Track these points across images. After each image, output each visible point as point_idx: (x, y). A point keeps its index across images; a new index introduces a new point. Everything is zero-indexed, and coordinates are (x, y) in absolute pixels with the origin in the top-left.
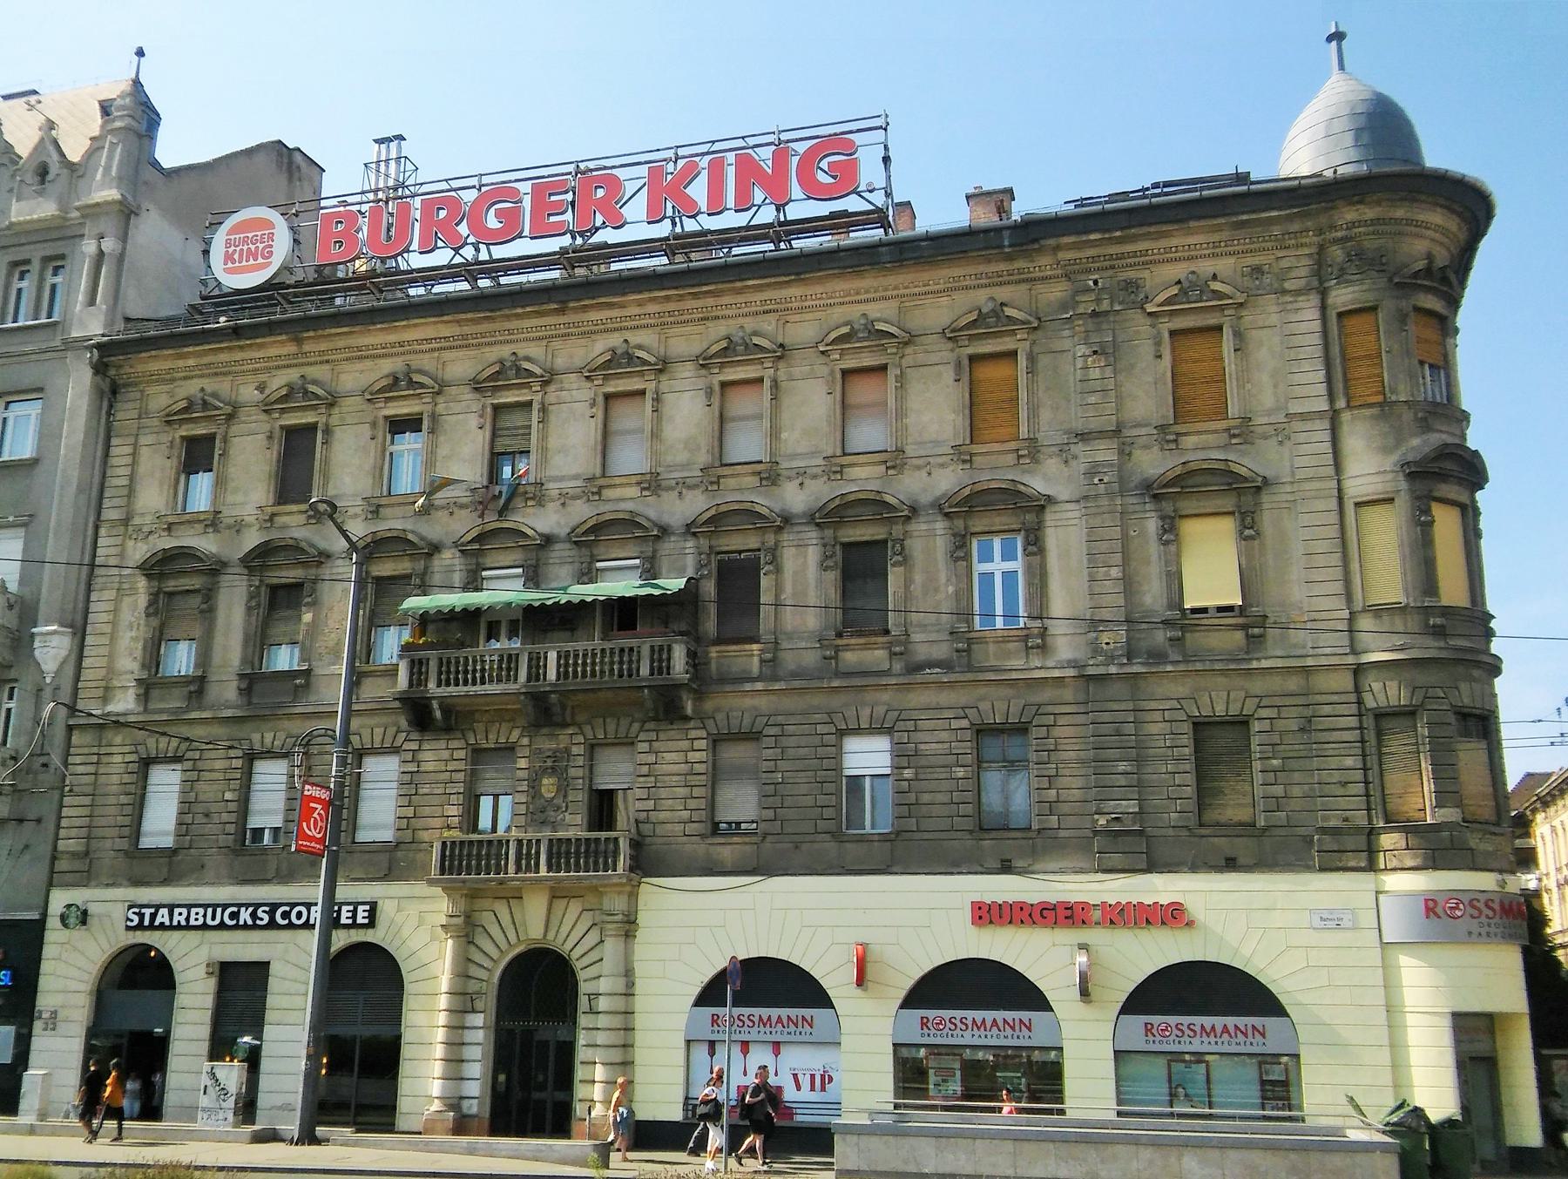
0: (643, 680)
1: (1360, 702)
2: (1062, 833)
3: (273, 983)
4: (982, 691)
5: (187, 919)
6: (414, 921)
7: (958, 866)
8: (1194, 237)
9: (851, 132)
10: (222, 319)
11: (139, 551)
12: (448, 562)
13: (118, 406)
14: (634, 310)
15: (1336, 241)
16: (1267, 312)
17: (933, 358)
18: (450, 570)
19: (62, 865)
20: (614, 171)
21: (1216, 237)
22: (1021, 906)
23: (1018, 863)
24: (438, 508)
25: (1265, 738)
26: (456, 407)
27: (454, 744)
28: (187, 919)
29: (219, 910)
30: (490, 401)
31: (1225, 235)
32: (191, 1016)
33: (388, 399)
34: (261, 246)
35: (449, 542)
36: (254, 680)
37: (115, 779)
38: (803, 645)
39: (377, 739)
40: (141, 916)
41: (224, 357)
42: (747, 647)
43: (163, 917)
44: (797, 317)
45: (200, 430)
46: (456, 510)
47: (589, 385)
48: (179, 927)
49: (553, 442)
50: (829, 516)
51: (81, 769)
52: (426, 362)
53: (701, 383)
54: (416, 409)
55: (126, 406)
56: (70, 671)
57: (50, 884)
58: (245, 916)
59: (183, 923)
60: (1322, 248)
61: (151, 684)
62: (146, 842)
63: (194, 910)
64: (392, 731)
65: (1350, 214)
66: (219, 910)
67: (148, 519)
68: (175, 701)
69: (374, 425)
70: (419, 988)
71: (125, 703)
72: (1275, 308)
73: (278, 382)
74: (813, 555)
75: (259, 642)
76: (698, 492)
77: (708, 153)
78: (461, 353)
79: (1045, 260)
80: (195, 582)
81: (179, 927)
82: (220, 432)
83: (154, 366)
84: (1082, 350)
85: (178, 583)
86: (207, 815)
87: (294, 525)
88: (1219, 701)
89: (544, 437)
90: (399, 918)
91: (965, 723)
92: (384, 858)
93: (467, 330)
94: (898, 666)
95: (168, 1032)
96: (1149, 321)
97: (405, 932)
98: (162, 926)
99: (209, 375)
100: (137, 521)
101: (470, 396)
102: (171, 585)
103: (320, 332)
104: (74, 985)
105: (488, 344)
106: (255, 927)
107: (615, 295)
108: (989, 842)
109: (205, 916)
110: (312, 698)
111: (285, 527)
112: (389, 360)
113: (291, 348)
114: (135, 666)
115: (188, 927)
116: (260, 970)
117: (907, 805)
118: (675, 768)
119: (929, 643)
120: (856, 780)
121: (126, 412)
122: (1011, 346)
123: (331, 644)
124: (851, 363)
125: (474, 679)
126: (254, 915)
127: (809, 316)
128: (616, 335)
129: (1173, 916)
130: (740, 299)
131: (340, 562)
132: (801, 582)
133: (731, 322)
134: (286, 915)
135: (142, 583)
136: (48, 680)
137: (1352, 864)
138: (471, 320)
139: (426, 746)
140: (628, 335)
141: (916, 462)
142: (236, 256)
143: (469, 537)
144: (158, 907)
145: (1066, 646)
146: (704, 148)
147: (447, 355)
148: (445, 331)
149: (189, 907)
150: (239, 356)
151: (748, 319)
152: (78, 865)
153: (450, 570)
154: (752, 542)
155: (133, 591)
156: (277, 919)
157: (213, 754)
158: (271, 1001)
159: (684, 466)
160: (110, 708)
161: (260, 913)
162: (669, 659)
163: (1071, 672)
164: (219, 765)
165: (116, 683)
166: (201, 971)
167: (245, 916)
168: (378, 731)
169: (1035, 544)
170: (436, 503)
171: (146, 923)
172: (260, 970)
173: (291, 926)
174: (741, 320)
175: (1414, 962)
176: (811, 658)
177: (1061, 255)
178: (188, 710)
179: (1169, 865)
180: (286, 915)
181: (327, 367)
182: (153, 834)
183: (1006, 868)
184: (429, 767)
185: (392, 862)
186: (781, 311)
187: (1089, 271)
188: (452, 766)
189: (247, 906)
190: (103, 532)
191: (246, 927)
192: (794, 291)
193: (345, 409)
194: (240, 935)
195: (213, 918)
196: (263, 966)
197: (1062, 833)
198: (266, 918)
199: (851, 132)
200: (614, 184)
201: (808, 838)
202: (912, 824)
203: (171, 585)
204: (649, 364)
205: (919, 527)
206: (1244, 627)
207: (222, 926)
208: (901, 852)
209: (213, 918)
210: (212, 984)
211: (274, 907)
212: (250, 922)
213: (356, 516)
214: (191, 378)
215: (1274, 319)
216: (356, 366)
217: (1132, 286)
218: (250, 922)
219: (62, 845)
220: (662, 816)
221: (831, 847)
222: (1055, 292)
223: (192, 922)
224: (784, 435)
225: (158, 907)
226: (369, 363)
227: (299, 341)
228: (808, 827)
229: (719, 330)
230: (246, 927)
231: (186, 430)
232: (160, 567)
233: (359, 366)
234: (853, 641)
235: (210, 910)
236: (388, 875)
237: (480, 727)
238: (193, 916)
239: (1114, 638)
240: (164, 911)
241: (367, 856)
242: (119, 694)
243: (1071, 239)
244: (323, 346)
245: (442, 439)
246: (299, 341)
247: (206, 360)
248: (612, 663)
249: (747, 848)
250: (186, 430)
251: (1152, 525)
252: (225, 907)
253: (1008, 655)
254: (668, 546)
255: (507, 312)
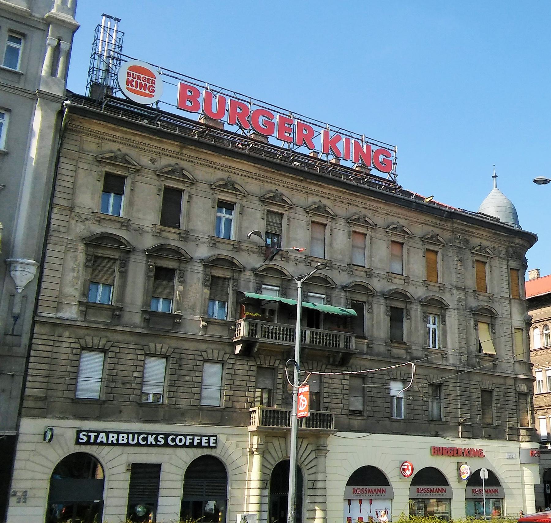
0: (307, 345)
1: (515, 389)
2: (451, 424)
3: (163, 475)
4: (430, 370)
5: (118, 440)
6: (234, 446)
7: (423, 433)
8: (484, 233)
9: (343, 134)
10: (146, 121)
11: (79, 229)
12: (248, 277)
13: (66, 140)
14: (328, 191)
15: (512, 247)
16: (495, 262)
17: (417, 246)
18: (248, 281)
19: (28, 403)
20: (389, 151)
21: (489, 235)
22: (445, 449)
23: (440, 433)
24: (243, 250)
25: (498, 397)
26: (252, 206)
27: (251, 363)
28: (118, 440)
29: (136, 436)
30: (266, 208)
31: (491, 235)
32: (116, 493)
33: (167, 178)
34: (148, 85)
35: (248, 267)
36: (150, 316)
37: (64, 356)
38: (380, 343)
39: (216, 356)
40: (89, 437)
41: (138, 139)
42: (363, 340)
43: (102, 437)
44: (378, 215)
45: (118, 172)
46: (251, 254)
47: (306, 215)
48: (112, 444)
49: (292, 235)
50: (389, 296)
51: (41, 348)
52: (237, 179)
53: (347, 229)
54: (234, 200)
55: (73, 142)
56: (34, 287)
57: (20, 415)
58: (151, 439)
59: (115, 442)
60: (508, 247)
61: (87, 307)
62: (81, 395)
63: (121, 435)
64: (222, 352)
65: (517, 241)
66: (136, 436)
67: (85, 211)
68: (103, 318)
69: (214, 201)
70: (234, 478)
71: (71, 313)
72: (498, 262)
73: (164, 161)
74: (383, 309)
75: (152, 295)
76: (345, 273)
77: (337, 132)
78: (254, 181)
79: (449, 224)
80: (116, 255)
81: (112, 444)
82: (187, 189)
83: (96, 128)
84: (456, 258)
85: (105, 252)
86: (124, 384)
87: (172, 238)
88: (487, 385)
89: (288, 231)
90: (227, 444)
91: (426, 381)
92: (219, 414)
93: (261, 173)
94: (408, 357)
95: (102, 502)
96: (471, 255)
97: (230, 451)
98: (102, 443)
99: (126, 144)
100: (78, 210)
101: (258, 202)
102: (100, 252)
103: (197, 149)
104: (38, 476)
105: (267, 182)
106: (157, 446)
107: (325, 183)
108: (432, 426)
109: (128, 439)
110: (182, 330)
111: (167, 238)
112: (222, 172)
113: (178, 150)
114: (77, 294)
115: (118, 444)
116: (157, 468)
117: (410, 409)
118: (338, 386)
119: (417, 352)
120: (393, 397)
121: (70, 145)
122: (437, 249)
123: (190, 304)
124: (394, 239)
125: (276, 337)
126: (156, 439)
127: (381, 216)
128: (479, 239)
129: (479, 454)
130: (364, 201)
131: (196, 264)
132: (377, 321)
133: (357, 208)
134: (173, 440)
135: (81, 247)
136: (20, 291)
137: (515, 439)
138: (264, 170)
139: (238, 362)
140: (321, 199)
141: (414, 283)
142: (134, 83)
143: (261, 269)
144: (99, 432)
145: (452, 360)
146: (337, 130)
147: (248, 180)
148: (252, 170)
149: (118, 433)
150: (147, 141)
151: (363, 210)
152: (40, 404)
153: (248, 281)
154: (364, 299)
155: (76, 250)
156: (168, 442)
157: (127, 351)
158: (162, 484)
159: (341, 261)
160: (60, 315)
161: (159, 438)
162: (349, 343)
163: (455, 368)
164: (130, 357)
165: (64, 300)
166: (123, 468)
167: (151, 439)
168: (216, 352)
169: (443, 321)
170: (242, 247)
171: (92, 440)
172: (157, 468)
173: (176, 446)
174: (361, 209)
175: (527, 469)
176: (382, 349)
177: (455, 225)
178: (111, 324)
179: (476, 436)
180: (173, 440)
181: (190, 164)
182: (83, 390)
183: (437, 435)
184: (240, 372)
185: (225, 416)
186: (375, 211)
187: (459, 232)
188: (250, 373)
189: (152, 434)
190: (55, 210)
191: (151, 445)
192: (381, 206)
193: (198, 188)
194: (145, 450)
195: (133, 440)
196: (158, 467)
197: (451, 424)
198: (163, 441)
199: (343, 134)
200: (311, 132)
201: (381, 419)
202: (412, 417)
203: (100, 252)
204: (330, 214)
205: (413, 306)
206: (493, 361)
207: (138, 444)
208: (410, 426)
209: (133, 440)
210: (128, 475)
211: (167, 436)
212: (154, 443)
213: (204, 243)
214: (114, 141)
215: (498, 265)
216: (206, 170)
217: (467, 241)
218: (154, 443)
219: (28, 392)
220: (333, 405)
221: (388, 423)
222: (448, 235)
223: (120, 442)
224: (373, 259)
225: (99, 432)
226: (211, 170)
227: (182, 148)
228: (381, 415)
229: (353, 210)
230: (151, 445)
231: (108, 169)
232: (94, 242)
233: (206, 169)
234: (396, 345)
235: (131, 436)
236: (221, 422)
237: (262, 357)
238: (121, 438)
239: (464, 358)
240: (103, 435)
241: (210, 413)
242: (66, 308)
243: (460, 222)
244: (193, 154)
245: (245, 218)
246: (182, 148)
247: (127, 136)
248: (320, 338)
249: (363, 422)
250: (108, 169)
251: (472, 322)
252: (139, 434)
253: (437, 358)
254: (336, 293)
255: (283, 173)
